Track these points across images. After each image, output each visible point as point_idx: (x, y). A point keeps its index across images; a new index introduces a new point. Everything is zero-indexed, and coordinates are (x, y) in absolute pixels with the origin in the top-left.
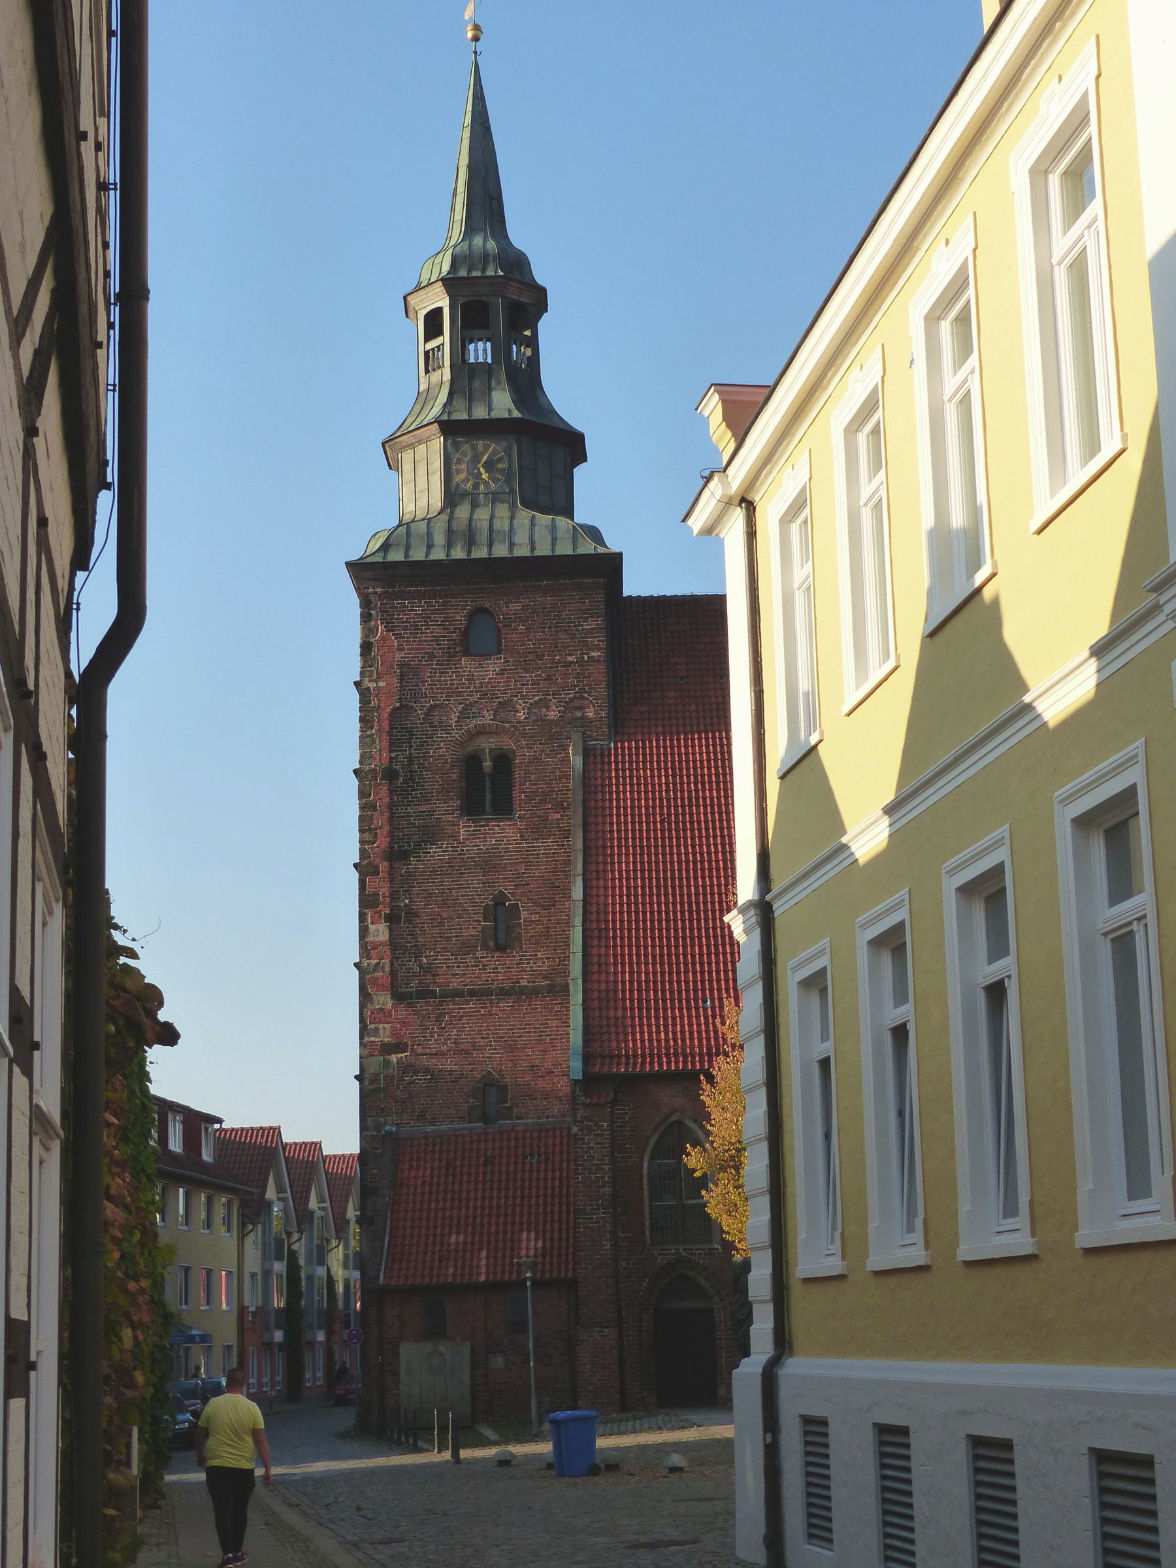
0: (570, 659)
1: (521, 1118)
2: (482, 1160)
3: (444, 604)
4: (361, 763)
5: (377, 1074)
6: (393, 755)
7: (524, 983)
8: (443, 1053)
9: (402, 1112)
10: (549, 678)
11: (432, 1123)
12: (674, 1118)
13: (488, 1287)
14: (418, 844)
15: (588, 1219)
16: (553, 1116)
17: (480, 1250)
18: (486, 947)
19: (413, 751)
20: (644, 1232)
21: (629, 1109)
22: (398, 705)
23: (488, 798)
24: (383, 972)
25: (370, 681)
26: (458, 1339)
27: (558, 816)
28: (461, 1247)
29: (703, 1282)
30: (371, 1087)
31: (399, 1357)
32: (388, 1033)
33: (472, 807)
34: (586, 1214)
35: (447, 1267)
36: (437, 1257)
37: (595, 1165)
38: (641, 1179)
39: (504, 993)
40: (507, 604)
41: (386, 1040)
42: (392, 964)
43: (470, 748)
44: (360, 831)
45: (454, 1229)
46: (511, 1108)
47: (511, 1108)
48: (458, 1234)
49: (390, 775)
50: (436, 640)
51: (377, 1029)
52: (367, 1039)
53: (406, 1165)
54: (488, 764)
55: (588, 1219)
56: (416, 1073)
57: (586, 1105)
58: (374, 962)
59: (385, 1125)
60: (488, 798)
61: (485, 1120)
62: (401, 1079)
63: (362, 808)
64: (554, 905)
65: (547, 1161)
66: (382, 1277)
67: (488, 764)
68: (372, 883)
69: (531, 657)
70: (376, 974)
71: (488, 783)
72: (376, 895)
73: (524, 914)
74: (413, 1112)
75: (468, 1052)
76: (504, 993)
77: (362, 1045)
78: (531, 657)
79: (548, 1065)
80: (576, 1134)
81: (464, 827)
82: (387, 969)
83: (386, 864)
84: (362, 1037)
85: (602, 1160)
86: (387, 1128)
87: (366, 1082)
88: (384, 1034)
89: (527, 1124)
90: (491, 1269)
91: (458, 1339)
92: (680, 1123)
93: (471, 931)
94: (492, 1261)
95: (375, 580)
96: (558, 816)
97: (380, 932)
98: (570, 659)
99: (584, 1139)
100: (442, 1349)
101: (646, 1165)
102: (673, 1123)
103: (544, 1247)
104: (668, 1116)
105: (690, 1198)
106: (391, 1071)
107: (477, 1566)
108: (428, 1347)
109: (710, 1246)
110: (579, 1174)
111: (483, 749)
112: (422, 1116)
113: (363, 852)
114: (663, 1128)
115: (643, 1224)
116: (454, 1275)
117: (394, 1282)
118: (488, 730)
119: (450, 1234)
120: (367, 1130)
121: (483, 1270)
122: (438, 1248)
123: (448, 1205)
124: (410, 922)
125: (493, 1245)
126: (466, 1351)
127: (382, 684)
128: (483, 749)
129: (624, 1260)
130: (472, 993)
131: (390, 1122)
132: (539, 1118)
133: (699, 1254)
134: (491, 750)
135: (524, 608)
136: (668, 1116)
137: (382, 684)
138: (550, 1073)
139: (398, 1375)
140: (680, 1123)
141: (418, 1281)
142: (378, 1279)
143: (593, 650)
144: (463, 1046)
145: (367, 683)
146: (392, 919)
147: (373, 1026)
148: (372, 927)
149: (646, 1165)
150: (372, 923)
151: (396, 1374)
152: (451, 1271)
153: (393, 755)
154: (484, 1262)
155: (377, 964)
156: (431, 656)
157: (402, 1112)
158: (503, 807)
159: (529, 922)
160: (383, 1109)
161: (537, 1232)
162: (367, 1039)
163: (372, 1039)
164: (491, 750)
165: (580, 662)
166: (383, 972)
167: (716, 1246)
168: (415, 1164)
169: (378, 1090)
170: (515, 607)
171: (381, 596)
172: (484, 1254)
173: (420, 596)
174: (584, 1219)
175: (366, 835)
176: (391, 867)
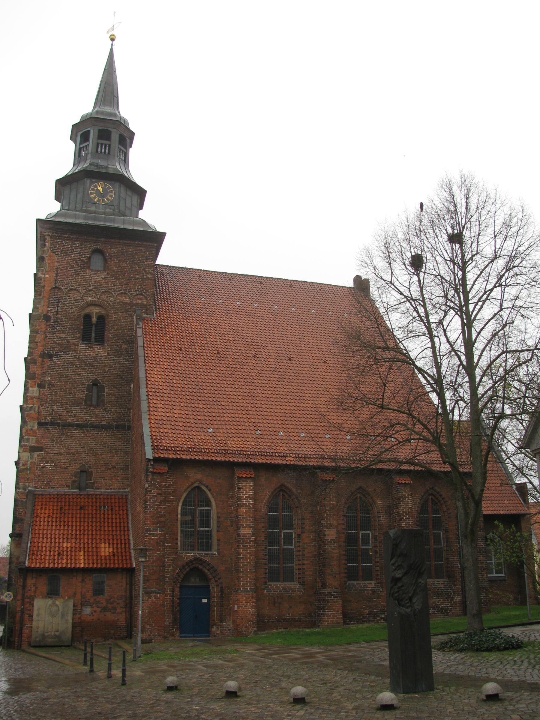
0: (137, 276)
1: (99, 489)
2: (79, 507)
3: (81, 245)
4: (33, 311)
5: (27, 461)
6: (49, 309)
7: (104, 423)
8: (61, 454)
9: (38, 481)
10: (127, 284)
11: (53, 488)
12: (195, 485)
13: (84, 571)
14: (57, 352)
15: (151, 534)
16: (114, 489)
17: (80, 551)
18: (86, 404)
19: (59, 309)
20: (177, 544)
21: (173, 478)
22: (54, 286)
23: (93, 335)
24: (35, 411)
25: (42, 274)
26: (66, 598)
27: (126, 346)
28: (69, 549)
29: (206, 571)
30: (23, 468)
31: (33, 606)
32: (34, 441)
33: (86, 338)
34: (151, 531)
35: (62, 559)
36: (56, 553)
37: (157, 505)
38: (177, 516)
39: (93, 427)
40: (111, 248)
41: (33, 444)
42: (39, 408)
43: (87, 311)
44: (29, 343)
45: (65, 540)
46: (93, 483)
47: (93, 483)
48: (68, 542)
49: (47, 318)
50: (75, 260)
51: (28, 439)
52: (23, 443)
53: (39, 507)
54: (94, 319)
55: (151, 534)
56: (47, 462)
57: (153, 473)
58: (30, 406)
59: (29, 486)
60: (93, 335)
61: (79, 488)
62: (39, 465)
63: (31, 332)
64: (121, 388)
65: (112, 509)
66: (27, 563)
67: (94, 319)
68: (33, 368)
69: (119, 273)
70: (31, 412)
71: (94, 328)
72: (35, 373)
73: (107, 390)
74: (43, 482)
75: (74, 454)
76: (93, 427)
77: (20, 446)
78: (119, 273)
79: (113, 464)
80: (148, 488)
81: (81, 347)
82: (37, 410)
83: (41, 359)
84: (20, 442)
85: (160, 503)
86: (29, 488)
87: (21, 465)
88: (32, 442)
89: (101, 492)
90: (86, 561)
91: (66, 598)
92: (198, 488)
93: (79, 396)
94: (86, 558)
95: (49, 229)
96: (126, 346)
97: (34, 391)
98: (137, 276)
99: (151, 491)
100: (57, 603)
101: (180, 508)
102: (195, 487)
103: (113, 552)
104: (193, 483)
105: (201, 527)
106: (34, 460)
107: (210, 718)
108: (50, 601)
109: (211, 552)
110: (148, 509)
111: (93, 312)
112: (48, 484)
113: (30, 353)
114: (189, 489)
115: (177, 539)
116: (67, 564)
117: (33, 565)
118: (96, 303)
119: (63, 542)
120: (19, 489)
121: (82, 561)
122: (57, 549)
123: (62, 528)
124: (50, 388)
125: (86, 550)
126: (71, 604)
127: (47, 276)
128: (93, 312)
129: (167, 558)
130: (78, 426)
131: (31, 486)
132: (107, 489)
133: (206, 556)
134: (96, 313)
135: (119, 252)
136: (193, 483)
137: (47, 276)
138: (114, 467)
139: (32, 616)
140: (198, 488)
141: (47, 565)
142: (25, 563)
143: (148, 274)
144: (71, 451)
145: (40, 275)
146: (41, 386)
147: (26, 437)
148: (31, 389)
149: (180, 508)
150: (31, 387)
151: (31, 616)
152: (65, 561)
153: (49, 309)
154: (82, 557)
155: (32, 407)
156: (73, 267)
157: (38, 481)
158: (100, 340)
159: (109, 394)
160: (28, 479)
161: (109, 544)
162: (23, 443)
163: (26, 444)
164: (96, 313)
165: (143, 279)
166: (35, 411)
167: (215, 553)
168: (44, 507)
169: (27, 469)
170: (113, 250)
171: (51, 237)
172: (82, 553)
173: (70, 239)
174: (149, 534)
175: (32, 345)
176: (43, 361)
